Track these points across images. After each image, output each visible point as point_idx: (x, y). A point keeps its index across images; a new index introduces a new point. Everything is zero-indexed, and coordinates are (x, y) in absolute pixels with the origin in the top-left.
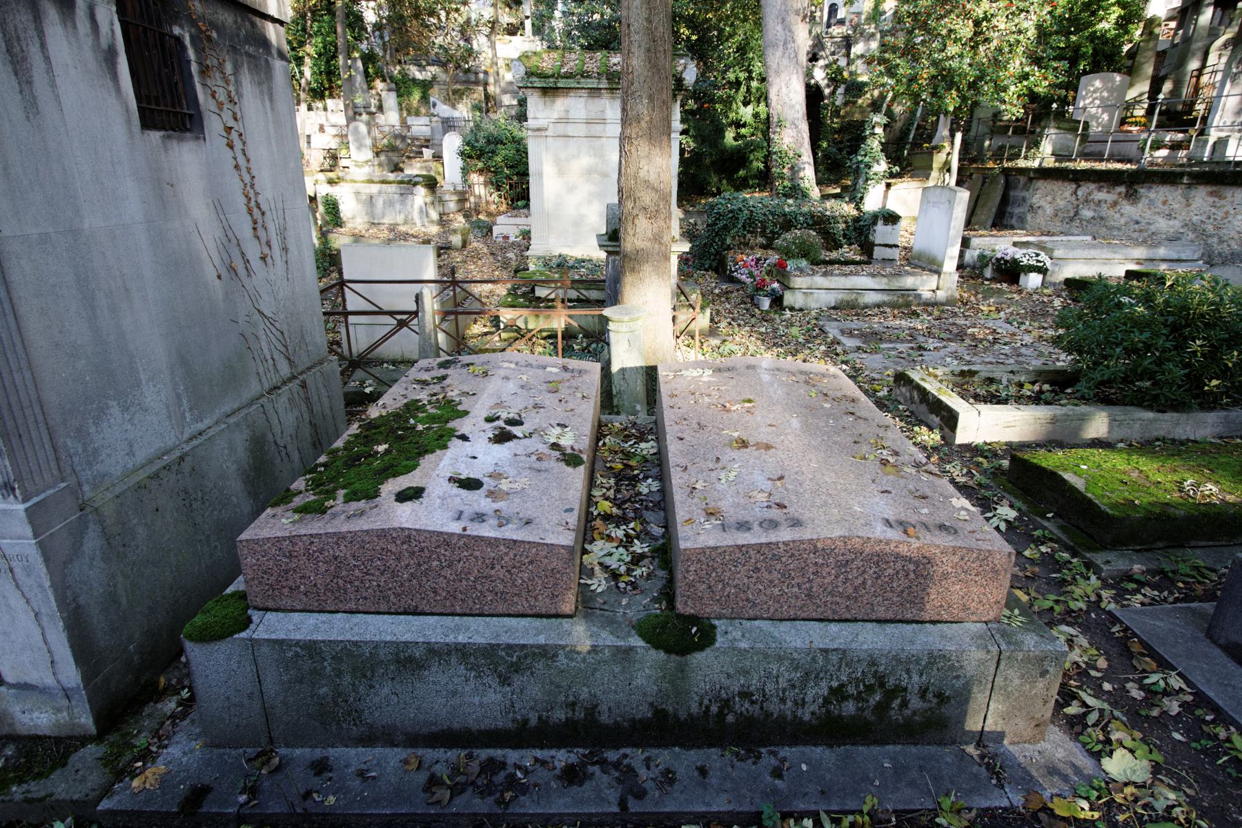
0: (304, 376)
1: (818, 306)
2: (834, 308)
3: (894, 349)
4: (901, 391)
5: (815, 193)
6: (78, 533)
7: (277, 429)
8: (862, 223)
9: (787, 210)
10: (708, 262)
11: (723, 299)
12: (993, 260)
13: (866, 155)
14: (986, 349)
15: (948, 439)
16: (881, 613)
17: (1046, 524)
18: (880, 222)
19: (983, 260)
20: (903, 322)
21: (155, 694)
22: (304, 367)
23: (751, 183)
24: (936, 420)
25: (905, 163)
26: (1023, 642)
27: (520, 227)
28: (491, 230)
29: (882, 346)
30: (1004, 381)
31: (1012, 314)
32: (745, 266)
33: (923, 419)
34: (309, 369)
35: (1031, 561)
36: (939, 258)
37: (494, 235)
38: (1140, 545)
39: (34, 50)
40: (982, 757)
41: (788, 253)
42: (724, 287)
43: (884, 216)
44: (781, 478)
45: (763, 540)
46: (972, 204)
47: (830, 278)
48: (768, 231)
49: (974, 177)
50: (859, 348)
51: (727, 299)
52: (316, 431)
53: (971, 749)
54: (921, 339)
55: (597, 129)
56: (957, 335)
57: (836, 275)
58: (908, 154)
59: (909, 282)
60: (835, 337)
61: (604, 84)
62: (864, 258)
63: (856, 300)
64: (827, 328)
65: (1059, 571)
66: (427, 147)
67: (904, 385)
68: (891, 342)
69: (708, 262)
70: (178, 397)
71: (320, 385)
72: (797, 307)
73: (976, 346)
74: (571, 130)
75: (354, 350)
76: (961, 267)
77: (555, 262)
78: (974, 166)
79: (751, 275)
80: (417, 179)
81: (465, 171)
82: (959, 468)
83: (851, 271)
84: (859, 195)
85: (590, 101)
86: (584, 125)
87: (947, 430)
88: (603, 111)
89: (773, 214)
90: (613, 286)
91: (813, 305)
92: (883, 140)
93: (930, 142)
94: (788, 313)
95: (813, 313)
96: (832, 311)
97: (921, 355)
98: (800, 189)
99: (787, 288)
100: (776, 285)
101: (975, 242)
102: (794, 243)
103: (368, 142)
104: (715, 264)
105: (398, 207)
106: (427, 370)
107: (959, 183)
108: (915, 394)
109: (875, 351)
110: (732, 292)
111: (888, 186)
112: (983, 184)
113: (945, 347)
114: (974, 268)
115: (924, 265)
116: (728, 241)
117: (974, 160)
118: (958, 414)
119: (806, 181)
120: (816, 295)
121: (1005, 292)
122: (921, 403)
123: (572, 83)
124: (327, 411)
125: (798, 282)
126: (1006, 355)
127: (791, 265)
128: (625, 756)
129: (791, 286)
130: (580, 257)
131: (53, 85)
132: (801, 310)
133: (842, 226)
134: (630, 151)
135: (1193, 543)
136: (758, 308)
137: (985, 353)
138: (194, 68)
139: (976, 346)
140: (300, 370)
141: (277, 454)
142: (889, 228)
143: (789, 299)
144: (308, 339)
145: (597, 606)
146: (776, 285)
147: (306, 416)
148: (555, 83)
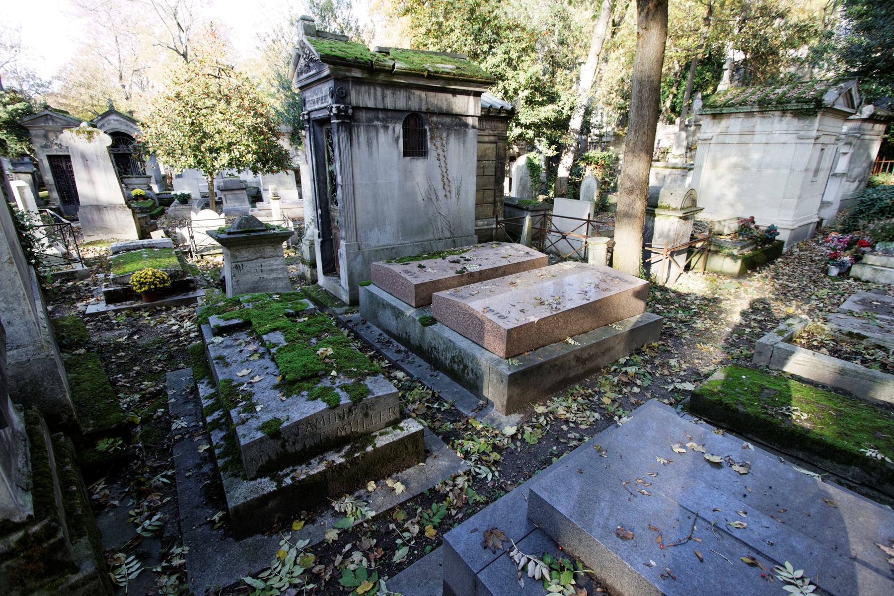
6: (356, 255)
16: (473, 339)
21: (453, 370)
38: (709, 418)
39: (375, 141)
45: (345, 249)
61: (756, 108)
70: (398, 232)
74: (728, 139)
85: (746, 120)
88: (754, 126)
103: (685, 143)
105: (679, 183)
120: (887, 273)
123: (733, 110)
131: (378, 148)
135: (750, 436)
138: (429, 137)
143: (856, 270)
148: (721, 110)
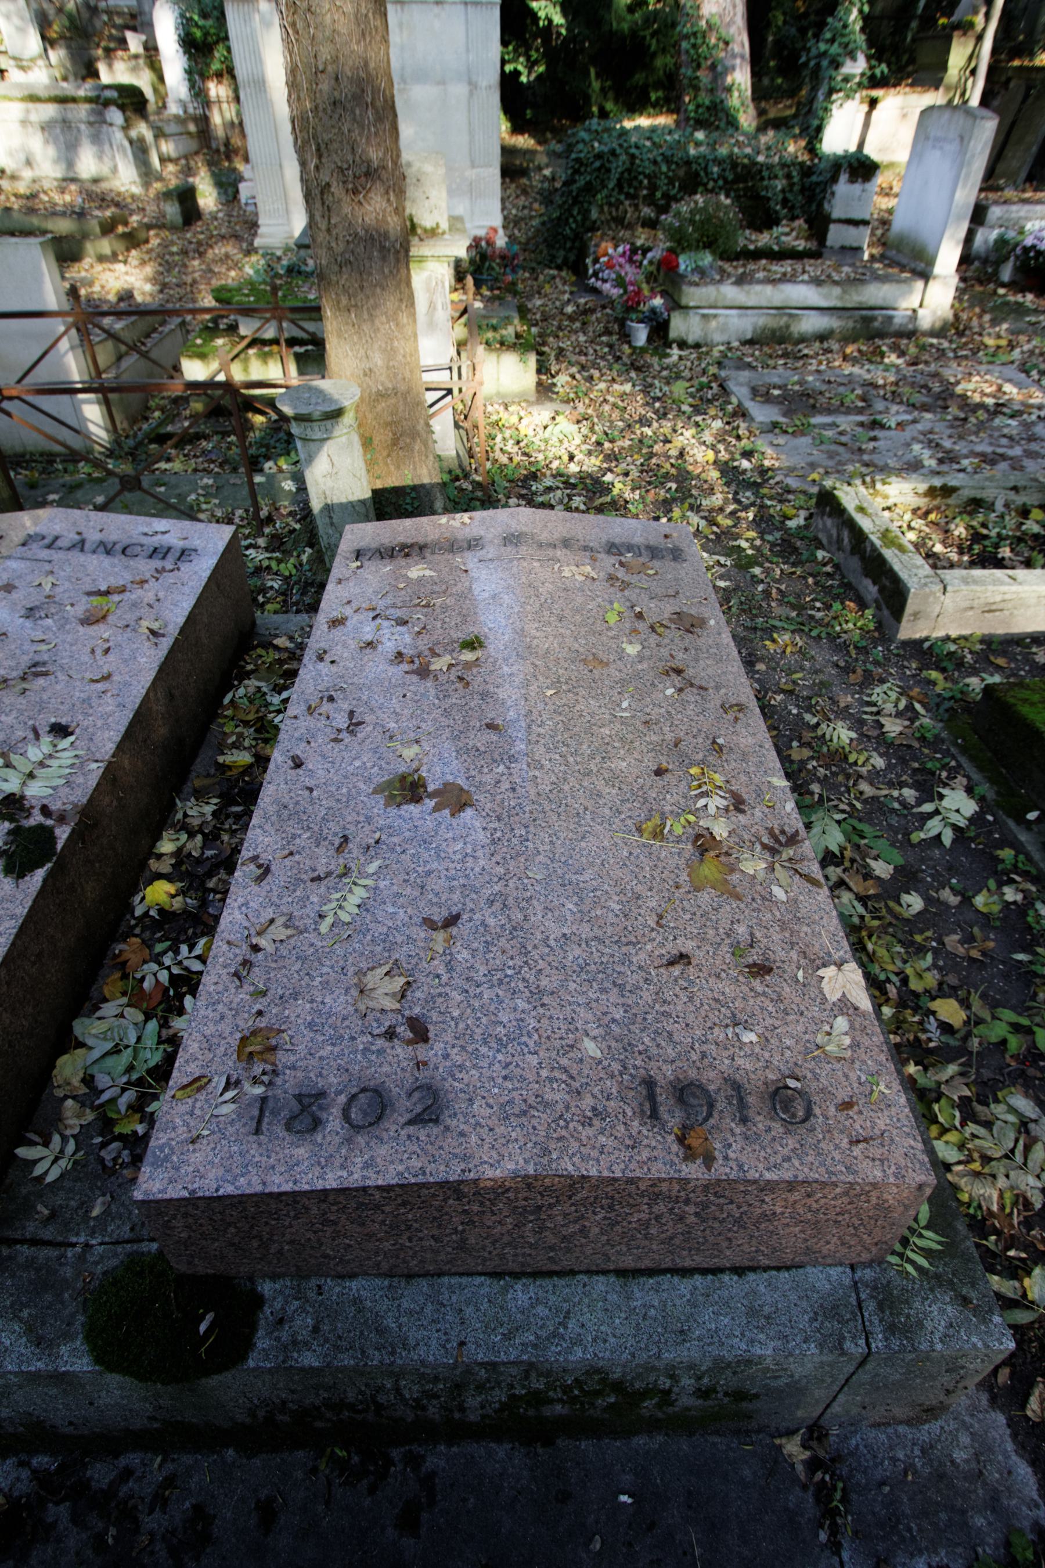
1: (724, 338)
2: (751, 342)
4: (824, 524)
5: (747, 119)
8: (814, 178)
9: (692, 151)
10: (562, 253)
11: (578, 325)
12: (1018, 251)
13: (832, 41)
14: (981, 426)
15: (884, 632)
17: (1023, 837)
18: (844, 177)
19: (1003, 248)
20: (856, 370)
23: (653, 97)
24: (870, 590)
25: (905, 57)
26: (920, 1324)
29: (814, 421)
30: (999, 506)
31: (1031, 352)
32: (610, 266)
33: (853, 580)
35: (986, 919)
36: (931, 249)
37: (243, 201)
40: (813, 1465)
41: (681, 243)
42: (582, 301)
43: (850, 165)
44: (452, 920)
46: (1002, 138)
47: (746, 287)
48: (658, 194)
49: (1012, 85)
50: (775, 425)
51: (584, 324)
53: (793, 1448)
54: (880, 405)
56: (939, 397)
57: (760, 282)
58: (914, 40)
59: (874, 293)
60: (740, 405)
62: (812, 245)
63: (788, 327)
64: (731, 385)
65: (1026, 949)
66: (134, 29)
67: (830, 515)
68: (829, 411)
69: (562, 253)
72: (691, 339)
73: (965, 420)
76: (965, 260)
78: (1016, 63)
79: (620, 282)
82: (894, 695)
83: (784, 274)
84: (816, 122)
87: (886, 612)
89: (668, 160)
91: (718, 338)
93: (949, 14)
94: (675, 352)
95: (715, 353)
96: (747, 349)
97: (874, 439)
98: (723, 110)
100: (658, 302)
101: (995, 212)
102: (692, 221)
104: (572, 257)
107: (984, 102)
108: (846, 535)
110: (592, 311)
111: (873, 103)
112: (1024, 101)
113: (915, 421)
114: (985, 261)
115: (905, 261)
116: (594, 214)
117: (1017, 53)
118: (908, 591)
119: (736, 94)
120: (721, 320)
121: (1028, 312)
122: (853, 552)
125: (692, 295)
126: (1011, 438)
128: (127, 1473)
132: (697, 346)
133: (779, 184)
136: (629, 343)
137: (976, 433)
139: (965, 420)
142: (857, 187)
143: (679, 326)
145: (31, 1228)
146: (658, 302)
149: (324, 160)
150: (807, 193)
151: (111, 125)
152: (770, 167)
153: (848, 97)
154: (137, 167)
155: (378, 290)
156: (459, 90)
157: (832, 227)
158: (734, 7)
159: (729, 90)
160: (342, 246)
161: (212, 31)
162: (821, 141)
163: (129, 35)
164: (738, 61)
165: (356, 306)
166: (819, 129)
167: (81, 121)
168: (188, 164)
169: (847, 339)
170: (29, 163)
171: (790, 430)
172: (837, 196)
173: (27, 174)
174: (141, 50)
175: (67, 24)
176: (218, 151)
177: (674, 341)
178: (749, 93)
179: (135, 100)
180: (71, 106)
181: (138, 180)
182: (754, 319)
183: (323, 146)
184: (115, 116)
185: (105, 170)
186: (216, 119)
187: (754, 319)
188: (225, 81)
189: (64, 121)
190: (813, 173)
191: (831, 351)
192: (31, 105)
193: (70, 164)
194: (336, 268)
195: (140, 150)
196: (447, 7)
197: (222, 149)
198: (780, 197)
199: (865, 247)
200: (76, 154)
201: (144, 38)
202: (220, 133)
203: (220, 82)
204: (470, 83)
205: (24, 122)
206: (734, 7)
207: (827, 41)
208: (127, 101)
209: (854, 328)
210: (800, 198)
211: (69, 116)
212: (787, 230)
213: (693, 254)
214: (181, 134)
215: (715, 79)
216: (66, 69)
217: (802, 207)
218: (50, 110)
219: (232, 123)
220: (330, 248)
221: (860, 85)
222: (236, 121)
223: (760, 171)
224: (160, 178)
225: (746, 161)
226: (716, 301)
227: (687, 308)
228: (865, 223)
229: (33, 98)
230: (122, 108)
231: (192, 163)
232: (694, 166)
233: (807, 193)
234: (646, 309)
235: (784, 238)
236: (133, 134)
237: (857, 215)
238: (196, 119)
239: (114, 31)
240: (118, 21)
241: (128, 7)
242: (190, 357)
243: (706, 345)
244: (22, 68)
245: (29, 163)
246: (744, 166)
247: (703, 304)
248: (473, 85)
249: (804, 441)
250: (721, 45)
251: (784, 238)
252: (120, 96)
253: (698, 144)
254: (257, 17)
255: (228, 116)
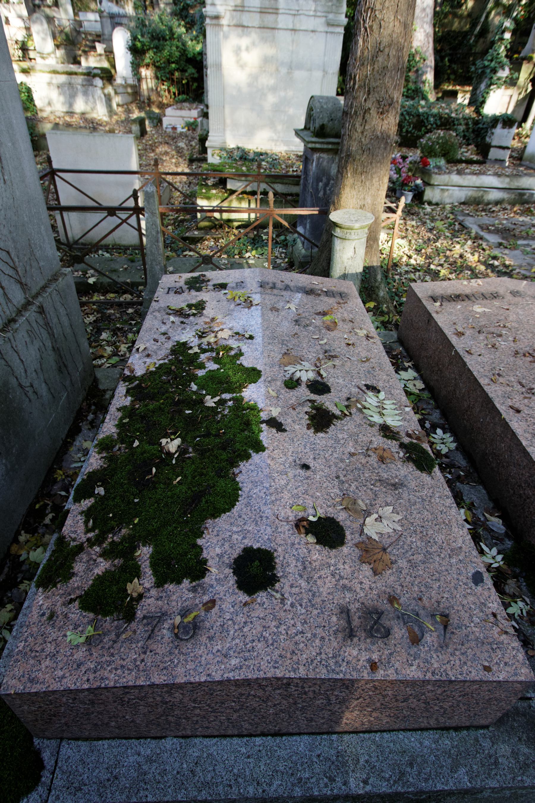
0: (40, 299)
2: (464, 203)
3: (528, 245)
7: (19, 370)
8: (481, 126)
9: (421, 110)
13: (492, 61)
18: (499, 126)
22: (38, 288)
27: (185, 119)
28: (160, 121)
34: (44, 288)
37: (164, 126)
47: (464, 176)
50: (500, 244)
52: (60, 355)
55: (269, 19)
60: (477, 233)
63: (482, 196)
66: (99, 42)
68: (525, 239)
71: (58, 305)
72: (434, 201)
75: (70, 235)
77: (237, 155)
80: (96, 71)
81: (136, 66)
86: (258, 15)
89: (409, 114)
90: (315, 184)
91: (447, 200)
92: (509, 46)
99: (427, 184)
100: (419, 182)
106: (179, 291)
109: (515, 247)
119: (427, 85)
120: (450, 192)
124: (68, 330)
125: (437, 179)
127: (432, 162)
129: (432, 182)
130: (259, 150)
132: (437, 204)
134: (371, 27)
140: (34, 291)
141: (24, 397)
142: (506, 131)
143: (429, 194)
144: (38, 254)
147: (49, 344)
149: (370, 96)
150: (476, 133)
151: (96, 86)
152: (458, 120)
153: (499, 87)
154: (107, 108)
155: (379, 164)
156: (318, 74)
157: (492, 150)
158: (429, 43)
159: (424, 82)
160: (368, 141)
161: (147, 44)
162: (483, 108)
163: (97, 44)
164: (429, 69)
165: (366, 172)
166: (483, 102)
167: (79, 84)
168: (128, 108)
169: (513, 204)
170: (49, 104)
171: (509, 247)
172: (495, 134)
173: (48, 109)
174: (103, 52)
175: (65, 38)
176: (144, 102)
177: (426, 201)
178: (433, 85)
179: (108, 75)
180: (74, 76)
181: (107, 114)
182: (467, 192)
183: (372, 89)
184: (98, 82)
185: (88, 109)
186: (144, 86)
187: (467, 192)
188: (150, 69)
189: (70, 84)
190: (479, 123)
191: (507, 209)
192: (53, 75)
193: (71, 105)
194: (360, 152)
195: (108, 99)
196: (317, 33)
197: (146, 101)
198: (462, 134)
199: (507, 160)
200: (75, 100)
201: (105, 46)
202: (146, 93)
203: (147, 69)
204: (324, 71)
205: (49, 84)
206: (429, 43)
207: (489, 61)
208: (105, 75)
209: (515, 198)
210: (472, 135)
211: (73, 81)
212: (466, 150)
213: (434, 159)
214: (124, 93)
215: (417, 77)
216: (64, 59)
217: (473, 139)
218: (63, 78)
219: (152, 89)
220: (361, 142)
221: (505, 82)
222: (154, 88)
223: (453, 121)
224: (116, 114)
225: (446, 116)
226: (448, 182)
227: (433, 185)
228: (508, 148)
229: (55, 72)
230: (102, 78)
231: (130, 107)
232: (422, 117)
233: (476, 133)
234: (413, 185)
235: (465, 154)
236: (106, 91)
237: (504, 144)
238: (133, 87)
239: (88, 43)
240: (90, 38)
241: (95, 32)
242: (202, 198)
243: (441, 204)
244: (43, 58)
245: (49, 104)
246: (445, 118)
247: (442, 184)
248: (325, 72)
249: (517, 252)
250: (422, 61)
251: (465, 154)
252: (102, 73)
253: (423, 107)
254: (222, 33)
255: (150, 86)
